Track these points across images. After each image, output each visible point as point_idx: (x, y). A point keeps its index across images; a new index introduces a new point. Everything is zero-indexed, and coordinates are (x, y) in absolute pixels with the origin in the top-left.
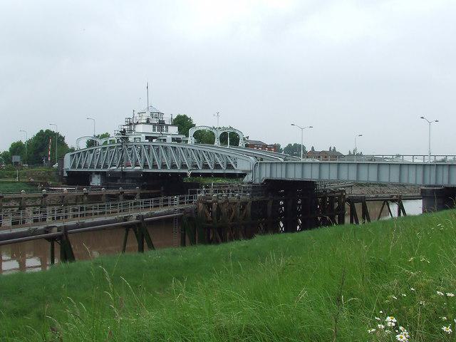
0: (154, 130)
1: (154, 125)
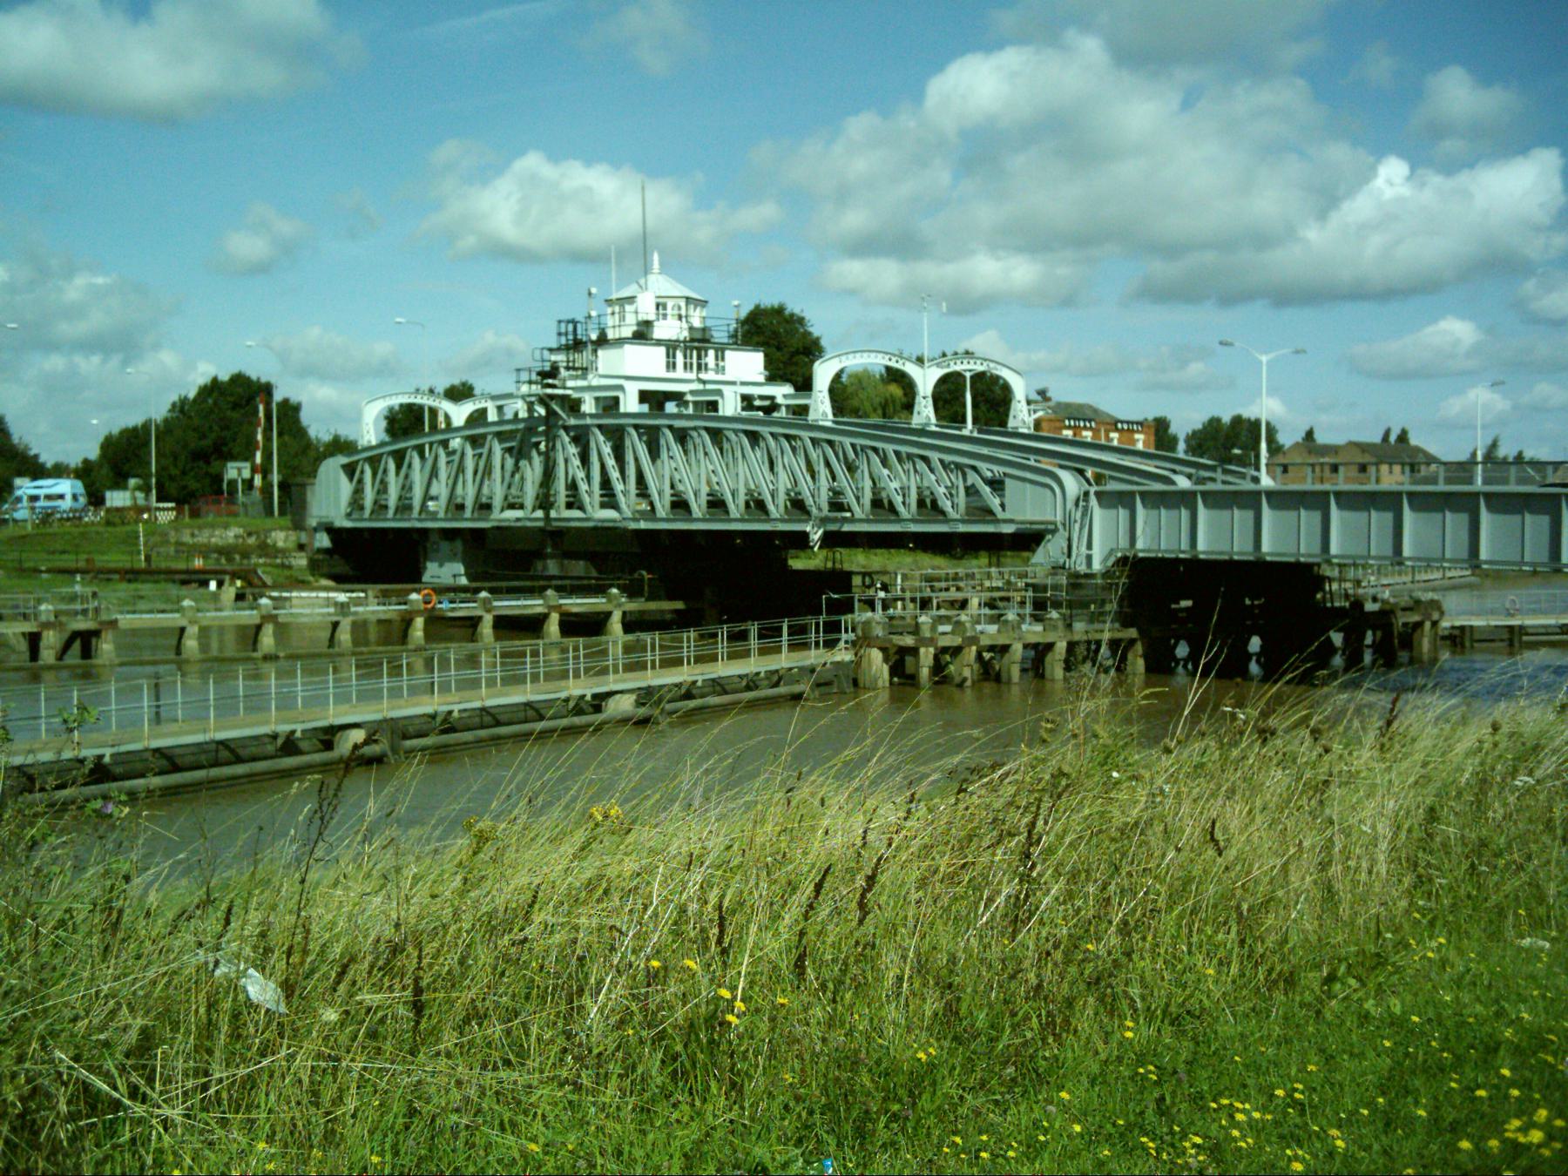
0: (671, 366)
1: (671, 346)
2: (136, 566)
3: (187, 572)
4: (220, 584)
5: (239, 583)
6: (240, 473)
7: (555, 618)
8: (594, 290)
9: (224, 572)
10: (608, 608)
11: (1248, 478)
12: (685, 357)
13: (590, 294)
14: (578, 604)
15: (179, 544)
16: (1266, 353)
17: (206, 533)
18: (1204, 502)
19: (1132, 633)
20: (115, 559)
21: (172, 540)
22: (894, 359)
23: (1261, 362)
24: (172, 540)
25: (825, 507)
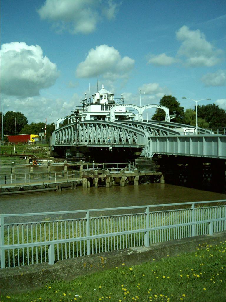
0: (102, 109)
1: (102, 105)
2: (13, 154)
3: (21, 155)
4: (27, 158)
5: (30, 158)
6: (42, 135)
7: (66, 167)
8: (86, 93)
9: (27, 156)
10: (80, 164)
11: (206, 131)
12: (106, 107)
13: (85, 94)
14: (71, 164)
15: (28, 149)
16: (197, 100)
17: (32, 147)
18: (192, 139)
19: (160, 173)
20: (9, 153)
21: (27, 149)
22: (158, 106)
23: (196, 102)
24: (27, 149)
25: (113, 142)
